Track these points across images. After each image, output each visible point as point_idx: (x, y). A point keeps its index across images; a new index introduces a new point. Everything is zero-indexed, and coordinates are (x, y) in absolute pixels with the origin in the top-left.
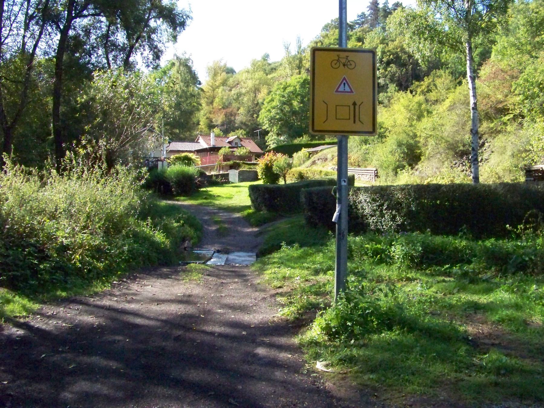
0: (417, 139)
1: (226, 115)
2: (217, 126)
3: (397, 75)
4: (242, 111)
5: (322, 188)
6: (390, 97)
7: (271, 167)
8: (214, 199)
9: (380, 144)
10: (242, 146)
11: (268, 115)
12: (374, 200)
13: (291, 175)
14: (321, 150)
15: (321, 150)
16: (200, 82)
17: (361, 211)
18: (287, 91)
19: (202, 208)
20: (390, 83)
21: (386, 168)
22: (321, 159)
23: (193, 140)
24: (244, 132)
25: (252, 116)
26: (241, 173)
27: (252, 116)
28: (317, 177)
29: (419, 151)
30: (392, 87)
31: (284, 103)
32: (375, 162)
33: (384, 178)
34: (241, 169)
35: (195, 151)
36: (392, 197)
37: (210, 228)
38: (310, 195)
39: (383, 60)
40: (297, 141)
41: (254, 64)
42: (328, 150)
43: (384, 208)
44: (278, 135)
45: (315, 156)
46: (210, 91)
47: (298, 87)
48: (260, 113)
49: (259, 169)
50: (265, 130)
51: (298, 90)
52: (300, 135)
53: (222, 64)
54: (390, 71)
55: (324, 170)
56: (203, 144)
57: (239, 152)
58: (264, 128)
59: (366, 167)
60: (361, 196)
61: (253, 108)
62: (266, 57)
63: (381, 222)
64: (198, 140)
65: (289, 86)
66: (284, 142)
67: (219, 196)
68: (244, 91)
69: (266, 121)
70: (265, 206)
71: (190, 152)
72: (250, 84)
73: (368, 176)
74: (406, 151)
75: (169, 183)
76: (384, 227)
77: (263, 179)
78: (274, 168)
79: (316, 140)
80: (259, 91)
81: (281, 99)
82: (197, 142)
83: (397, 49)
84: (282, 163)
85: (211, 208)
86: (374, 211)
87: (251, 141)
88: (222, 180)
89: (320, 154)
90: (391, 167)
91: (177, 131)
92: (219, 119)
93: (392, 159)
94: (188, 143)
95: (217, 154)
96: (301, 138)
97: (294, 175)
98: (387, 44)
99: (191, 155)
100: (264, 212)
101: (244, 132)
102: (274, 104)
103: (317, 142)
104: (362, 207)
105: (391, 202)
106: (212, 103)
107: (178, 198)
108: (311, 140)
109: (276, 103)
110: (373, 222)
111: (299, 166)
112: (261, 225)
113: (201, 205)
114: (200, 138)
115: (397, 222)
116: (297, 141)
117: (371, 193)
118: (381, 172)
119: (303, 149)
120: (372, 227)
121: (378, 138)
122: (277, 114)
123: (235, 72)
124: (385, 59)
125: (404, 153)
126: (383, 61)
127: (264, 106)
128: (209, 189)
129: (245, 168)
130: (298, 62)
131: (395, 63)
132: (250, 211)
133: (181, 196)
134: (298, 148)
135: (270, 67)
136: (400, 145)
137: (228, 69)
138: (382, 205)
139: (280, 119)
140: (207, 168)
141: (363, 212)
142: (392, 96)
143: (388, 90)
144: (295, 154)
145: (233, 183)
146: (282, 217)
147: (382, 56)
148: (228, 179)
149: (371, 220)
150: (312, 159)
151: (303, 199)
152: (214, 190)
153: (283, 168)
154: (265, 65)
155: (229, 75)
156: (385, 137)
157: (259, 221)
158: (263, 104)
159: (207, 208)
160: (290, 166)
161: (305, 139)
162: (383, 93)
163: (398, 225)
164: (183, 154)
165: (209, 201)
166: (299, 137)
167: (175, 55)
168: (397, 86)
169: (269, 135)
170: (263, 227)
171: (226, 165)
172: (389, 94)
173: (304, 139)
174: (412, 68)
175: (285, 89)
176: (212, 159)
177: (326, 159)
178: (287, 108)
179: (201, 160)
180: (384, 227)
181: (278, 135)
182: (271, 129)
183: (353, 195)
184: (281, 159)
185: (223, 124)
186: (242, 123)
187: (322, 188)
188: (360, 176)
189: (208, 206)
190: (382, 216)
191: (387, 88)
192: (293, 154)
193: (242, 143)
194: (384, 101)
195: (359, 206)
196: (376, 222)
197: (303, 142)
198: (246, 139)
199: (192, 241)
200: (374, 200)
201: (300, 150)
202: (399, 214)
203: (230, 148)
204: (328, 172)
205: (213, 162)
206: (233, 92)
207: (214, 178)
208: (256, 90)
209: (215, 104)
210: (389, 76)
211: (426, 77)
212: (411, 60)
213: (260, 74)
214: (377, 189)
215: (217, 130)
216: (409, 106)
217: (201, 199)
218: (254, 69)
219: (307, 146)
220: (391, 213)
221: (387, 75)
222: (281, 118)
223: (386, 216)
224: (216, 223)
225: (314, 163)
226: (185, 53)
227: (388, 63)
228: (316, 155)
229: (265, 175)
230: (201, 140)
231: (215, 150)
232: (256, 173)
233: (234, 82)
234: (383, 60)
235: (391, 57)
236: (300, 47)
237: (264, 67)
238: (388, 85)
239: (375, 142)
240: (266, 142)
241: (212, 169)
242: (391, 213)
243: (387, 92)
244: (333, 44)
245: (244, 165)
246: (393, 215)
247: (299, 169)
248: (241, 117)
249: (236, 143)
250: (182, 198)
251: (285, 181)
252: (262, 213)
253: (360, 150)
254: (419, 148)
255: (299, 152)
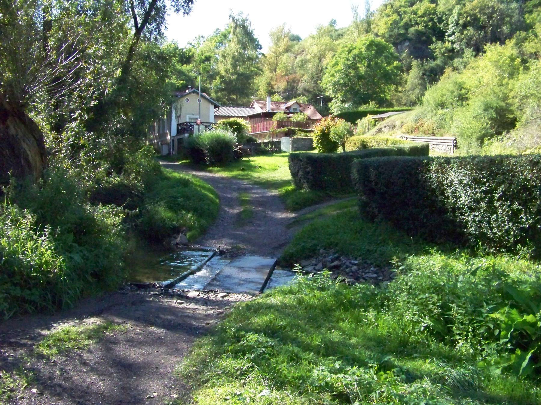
0: (510, 101)
1: (288, 82)
2: (278, 92)
3: (474, 38)
4: (305, 77)
5: (385, 158)
6: (466, 63)
7: (328, 134)
8: (252, 171)
9: (460, 109)
10: (301, 112)
11: (331, 80)
12: (477, 181)
13: (352, 144)
14: (388, 117)
15: (388, 117)
16: (261, 46)
17: (451, 200)
18: (352, 54)
19: (234, 181)
20: (466, 47)
21: (467, 136)
22: (388, 126)
23: (248, 105)
24: (306, 99)
25: (316, 82)
26: (294, 142)
27: (316, 82)
28: (383, 146)
29: (512, 116)
30: (468, 52)
31: (349, 67)
32: (454, 130)
33: (465, 149)
34: (295, 137)
35: (248, 116)
36: (513, 176)
37: (232, 211)
38: (364, 169)
39: (460, 22)
40: (362, 108)
41: (319, 30)
42: (396, 116)
43: (497, 196)
44: (343, 102)
45: (381, 123)
46: (273, 58)
47: (363, 50)
48: (323, 78)
49: (314, 137)
50: (328, 97)
51: (364, 52)
52: (366, 102)
53: (286, 30)
54: (467, 34)
55: (391, 138)
56: (258, 109)
57: (296, 118)
58: (327, 94)
59: (442, 135)
60: (452, 173)
61: (317, 74)
62: (333, 23)
63: (489, 222)
64: (253, 105)
65: (355, 48)
66: (348, 109)
67: (260, 167)
68: (308, 57)
69: (330, 86)
70: (307, 182)
71: (239, 117)
72: (315, 50)
73: (445, 147)
74: (495, 116)
75: (202, 151)
76: (495, 230)
77: (319, 148)
78: (332, 135)
79: (384, 107)
80: (324, 57)
81: (346, 62)
82: (252, 107)
83: (475, 10)
84: (341, 129)
85: (246, 182)
86: (477, 201)
87: (312, 108)
88: (271, 148)
89: (387, 121)
90: (475, 136)
91: (235, 97)
92: (282, 85)
93: (477, 126)
94: (242, 109)
95: (271, 120)
96: (368, 105)
97: (355, 144)
98: (464, 5)
99: (240, 120)
100: (305, 190)
101: (306, 99)
102: (338, 68)
103: (385, 109)
104: (453, 193)
105: (510, 187)
106: (275, 70)
107: (211, 168)
108: (379, 108)
109: (341, 67)
110: (474, 221)
111: (363, 134)
112: (301, 209)
113: (235, 178)
114: (255, 103)
115: (521, 223)
116: (362, 108)
117: (472, 169)
118: (461, 142)
119: (369, 116)
120: (472, 230)
121: (458, 101)
122: (342, 78)
123: (301, 40)
124: (461, 22)
125: (491, 119)
126: (458, 24)
127: (327, 71)
128: (251, 158)
129: (301, 135)
130: (365, 25)
131: (472, 25)
132: (290, 188)
133: (215, 166)
134: (363, 114)
135: (336, 33)
136: (487, 108)
137: (293, 36)
138: (492, 191)
139: (345, 85)
140: (256, 135)
141: (456, 202)
142: (469, 61)
143: (464, 55)
144: (358, 121)
145: (285, 152)
146: (330, 197)
147: (458, 17)
148: (280, 148)
149: (469, 217)
150: (378, 126)
151: (355, 175)
152: (258, 160)
153: (342, 135)
154: (332, 31)
155: (295, 42)
156: (467, 99)
157: (297, 204)
158: (327, 68)
159: (240, 181)
160: (351, 133)
161: (371, 106)
162: (459, 59)
163: (522, 230)
164: (232, 120)
165: (246, 172)
166: (365, 104)
167: (231, 16)
168: (474, 50)
169: (333, 102)
170: (304, 211)
171: (280, 132)
172: (465, 59)
173: (370, 106)
174: (492, 29)
175: (350, 51)
176: (265, 126)
177: (394, 127)
178: (353, 73)
179: (252, 127)
180: (495, 230)
181: (343, 102)
182: (335, 96)
183: (437, 171)
184: (341, 125)
185: (285, 90)
186: (305, 90)
187: (385, 158)
188: (435, 146)
189: (243, 179)
190: (494, 211)
191: (463, 53)
192: (356, 120)
193: (301, 109)
194: (459, 67)
195: (449, 193)
196: (480, 221)
197: (369, 110)
198: (306, 105)
199: (188, 234)
200: (477, 181)
201: (365, 116)
202: (527, 208)
203: (285, 113)
204: (396, 141)
205: (267, 129)
206: (298, 59)
207: (263, 146)
208: (321, 57)
209: (278, 71)
210: (465, 41)
211: (508, 40)
212: (491, 22)
213: (326, 40)
214: (482, 161)
215: (276, 97)
216: (498, 61)
217: (238, 170)
218: (319, 34)
219: (372, 113)
220: (509, 206)
221: (463, 39)
222: (345, 83)
223: (500, 211)
224: (242, 202)
225: (380, 130)
226: (242, 14)
227: (465, 26)
228: (383, 122)
229: (321, 143)
230: (256, 105)
231: (268, 115)
232: (311, 141)
233: (299, 49)
234: (460, 22)
235: (468, 18)
236: (368, 10)
237: (331, 33)
238: (463, 49)
239: (454, 106)
240: (329, 109)
241: (261, 136)
242: (509, 206)
243: (463, 58)
244: (404, 7)
245: (300, 132)
246: (513, 210)
247: (362, 137)
248: (304, 83)
249: (295, 109)
250: (216, 169)
251: (344, 149)
252: (303, 191)
253: (435, 115)
254: (512, 112)
255: (364, 119)
